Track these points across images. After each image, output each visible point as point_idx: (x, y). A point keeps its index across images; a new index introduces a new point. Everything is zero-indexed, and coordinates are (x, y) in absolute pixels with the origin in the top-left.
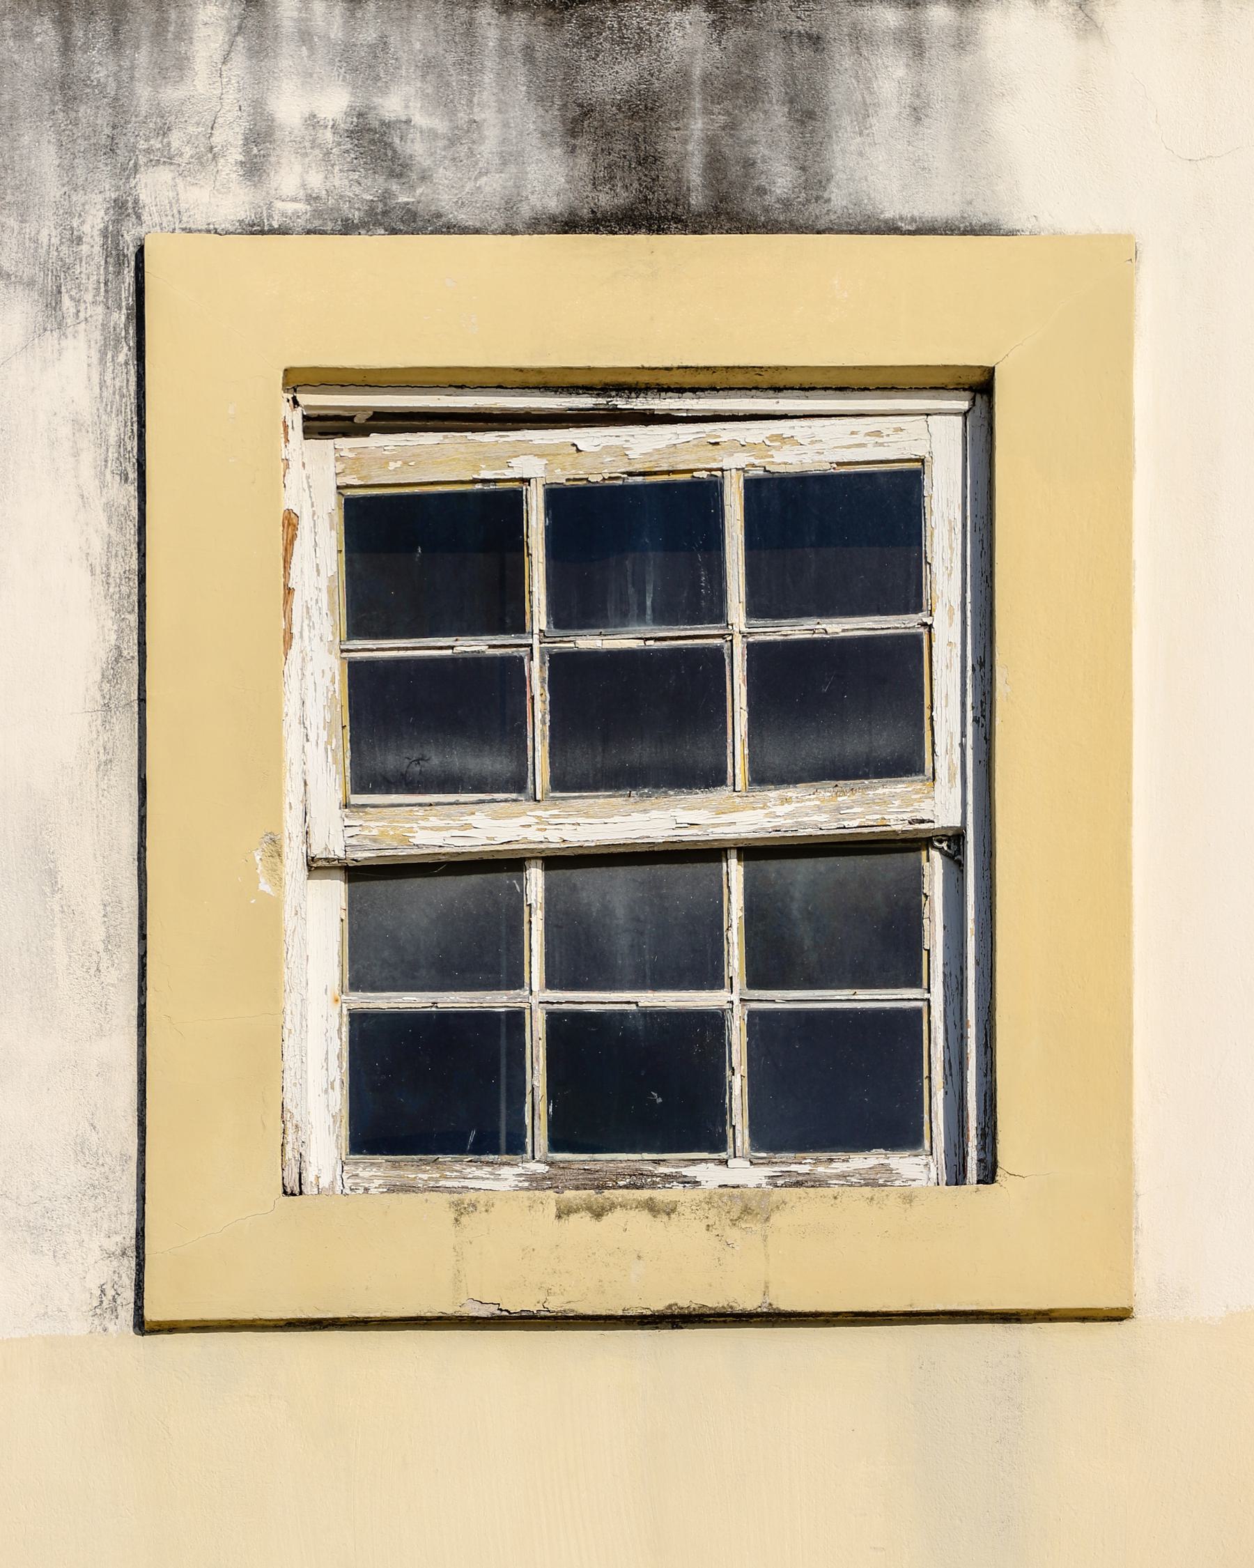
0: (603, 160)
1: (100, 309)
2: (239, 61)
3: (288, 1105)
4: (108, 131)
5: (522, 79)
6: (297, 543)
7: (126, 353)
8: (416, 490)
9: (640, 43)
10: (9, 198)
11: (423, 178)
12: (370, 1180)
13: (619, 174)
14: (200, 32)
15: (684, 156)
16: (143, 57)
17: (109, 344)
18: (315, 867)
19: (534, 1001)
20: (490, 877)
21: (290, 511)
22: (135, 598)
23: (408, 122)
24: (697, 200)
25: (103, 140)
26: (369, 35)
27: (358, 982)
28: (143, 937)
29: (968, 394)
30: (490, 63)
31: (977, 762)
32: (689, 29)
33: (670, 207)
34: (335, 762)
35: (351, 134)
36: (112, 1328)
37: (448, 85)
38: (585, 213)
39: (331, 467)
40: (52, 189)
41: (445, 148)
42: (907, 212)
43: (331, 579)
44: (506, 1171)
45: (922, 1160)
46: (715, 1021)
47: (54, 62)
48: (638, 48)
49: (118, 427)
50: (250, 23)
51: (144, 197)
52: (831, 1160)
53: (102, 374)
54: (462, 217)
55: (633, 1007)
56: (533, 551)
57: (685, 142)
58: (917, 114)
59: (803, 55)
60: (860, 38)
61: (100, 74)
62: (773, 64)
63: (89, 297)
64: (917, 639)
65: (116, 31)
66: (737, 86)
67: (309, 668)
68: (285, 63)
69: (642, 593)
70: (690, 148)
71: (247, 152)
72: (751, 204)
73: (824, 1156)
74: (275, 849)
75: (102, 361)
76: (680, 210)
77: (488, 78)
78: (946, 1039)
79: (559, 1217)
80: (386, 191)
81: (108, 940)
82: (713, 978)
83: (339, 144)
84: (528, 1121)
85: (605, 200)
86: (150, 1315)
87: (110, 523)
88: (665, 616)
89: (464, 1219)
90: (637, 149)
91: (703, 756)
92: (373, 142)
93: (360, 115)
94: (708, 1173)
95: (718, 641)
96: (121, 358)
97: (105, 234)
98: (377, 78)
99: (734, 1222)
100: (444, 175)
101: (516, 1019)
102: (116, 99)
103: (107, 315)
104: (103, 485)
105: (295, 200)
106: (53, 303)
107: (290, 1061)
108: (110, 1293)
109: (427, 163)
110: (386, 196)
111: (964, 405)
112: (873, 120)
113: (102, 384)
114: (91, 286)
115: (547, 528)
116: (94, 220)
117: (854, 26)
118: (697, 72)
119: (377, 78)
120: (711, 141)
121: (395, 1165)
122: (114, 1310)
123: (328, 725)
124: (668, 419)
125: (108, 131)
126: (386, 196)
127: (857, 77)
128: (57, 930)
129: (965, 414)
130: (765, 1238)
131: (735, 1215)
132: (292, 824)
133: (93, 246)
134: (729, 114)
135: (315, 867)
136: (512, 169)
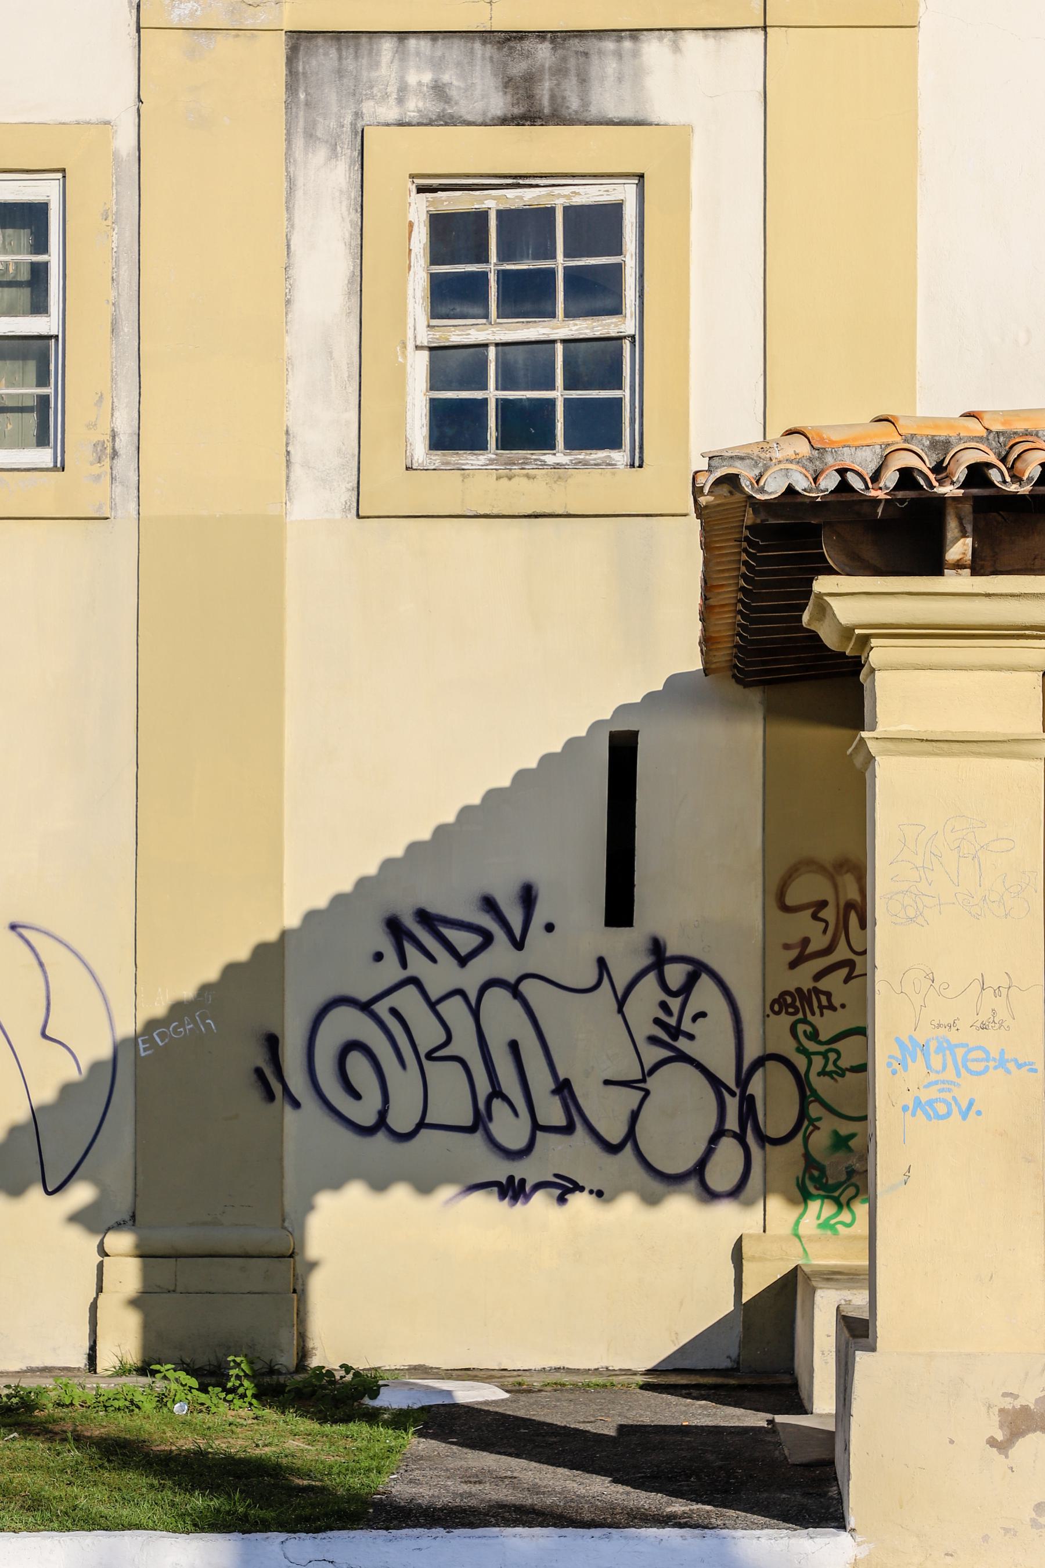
0: (516, 97)
1: (349, 151)
2: (396, 62)
3: (408, 436)
4: (353, 88)
5: (489, 68)
6: (413, 233)
7: (358, 166)
8: (453, 211)
9: (528, 55)
10: (321, 111)
11: (456, 104)
12: (436, 460)
13: (521, 102)
14: (384, 53)
15: (542, 95)
16: (364, 61)
17: (352, 164)
18: (417, 348)
19: (491, 395)
20: (477, 349)
21: (410, 222)
22: (359, 254)
23: (451, 84)
24: (547, 111)
25: (352, 91)
26: (439, 53)
27: (432, 388)
28: (360, 376)
29: (638, 178)
30: (479, 62)
31: (640, 312)
32: (545, 50)
33: (538, 113)
34: (425, 311)
35: (432, 88)
36: (349, 516)
37: (464, 70)
38: (509, 115)
39: (425, 204)
40: (334, 109)
41: (464, 92)
42: (616, 114)
43: (424, 244)
44: (481, 457)
45: (622, 454)
46: (552, 402)
47: (336, 64)
48: (528, 57)
49: (355, 193)
50: (400, 49)
51: (364, 111)
52: (591, 454)
53: (350, 174)
54: (469, 118)
55: (525, 397)
56: (492, 234)
57: (543, 90)
58: (620, 80)
59: (582, 59)
60: (600, 53)
61: (351, 68)
62: (572, 63)
63: (346, 147)
64: (621, 264)
65: (356, 52)
66: (560, 70)
67: (417, 276)
68: (412, 63)
69: (528, 249)
70: (544, 92)
71: (398, 95)
72: (564, 112)
73: (588, 452)
74: (404, 346)
75: (350, 169)
76: (541, 114)
77: (478, 68)
78: (630, 409)
79: (497, 479)
80: (444, 108)
81: (349, 377)
82: (552, 387)
83: (428, 92)
84: (489, 439)
85: (517, 111)
86: (361, 514)
87: (351, 227)
88: (537, 257)
89: (465, 480)
90: (527, 93)
91: (550, 309)
92: (439, 91)
93: (436, 81)
94: (549, 458)
95: (554, 266)
96: (356, 168)
97: (351, 124)
98: (441, 68)
99: (555, 482)
100: (463, 102)
101: (484, 402)
102: (356, 76)
103: (351, 153)
104: (349, 214)
105: (413, 111)
106: (334, 148)
107: (409, 420)
108: (349, 503)
109: (457, 98)
110: (444, 110)
111: (636, 182)
112: (605, 82)
113: (350, 177)
114: (347, 143)
115: (497, 225)
116: (348, 119)
117: (599, 49)
118: (547, 65)
119: (441, 68)
120: (551, 90)
121: (444, 455)
122: (350, 510)
123: (423, 298)
124: (537, 186)
125: (353, 88)
126: (444, 110)
127: (600, 67)
128: (332, 373)
129: (637, 184)
130: (565, 488)
131: (555, 479)
132: (410, 334)
133: (347, 128)
134: (557, 80)
135: (417, 348)
136: (485, 100)
